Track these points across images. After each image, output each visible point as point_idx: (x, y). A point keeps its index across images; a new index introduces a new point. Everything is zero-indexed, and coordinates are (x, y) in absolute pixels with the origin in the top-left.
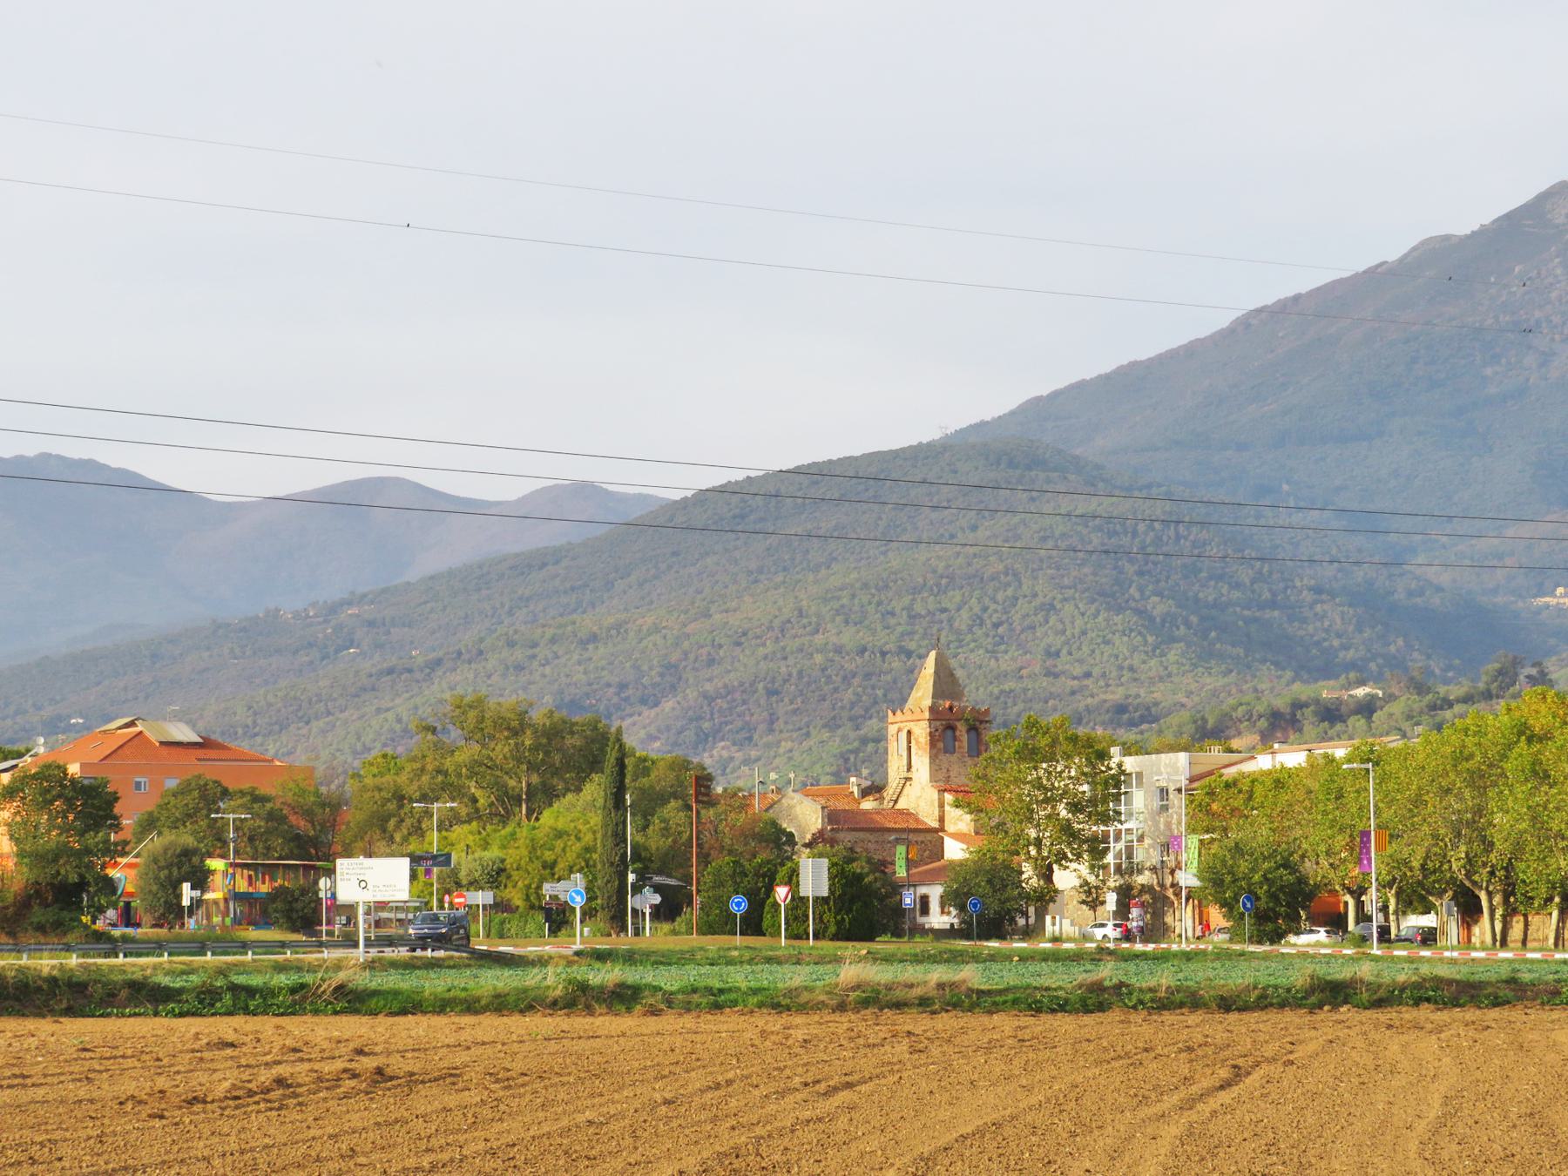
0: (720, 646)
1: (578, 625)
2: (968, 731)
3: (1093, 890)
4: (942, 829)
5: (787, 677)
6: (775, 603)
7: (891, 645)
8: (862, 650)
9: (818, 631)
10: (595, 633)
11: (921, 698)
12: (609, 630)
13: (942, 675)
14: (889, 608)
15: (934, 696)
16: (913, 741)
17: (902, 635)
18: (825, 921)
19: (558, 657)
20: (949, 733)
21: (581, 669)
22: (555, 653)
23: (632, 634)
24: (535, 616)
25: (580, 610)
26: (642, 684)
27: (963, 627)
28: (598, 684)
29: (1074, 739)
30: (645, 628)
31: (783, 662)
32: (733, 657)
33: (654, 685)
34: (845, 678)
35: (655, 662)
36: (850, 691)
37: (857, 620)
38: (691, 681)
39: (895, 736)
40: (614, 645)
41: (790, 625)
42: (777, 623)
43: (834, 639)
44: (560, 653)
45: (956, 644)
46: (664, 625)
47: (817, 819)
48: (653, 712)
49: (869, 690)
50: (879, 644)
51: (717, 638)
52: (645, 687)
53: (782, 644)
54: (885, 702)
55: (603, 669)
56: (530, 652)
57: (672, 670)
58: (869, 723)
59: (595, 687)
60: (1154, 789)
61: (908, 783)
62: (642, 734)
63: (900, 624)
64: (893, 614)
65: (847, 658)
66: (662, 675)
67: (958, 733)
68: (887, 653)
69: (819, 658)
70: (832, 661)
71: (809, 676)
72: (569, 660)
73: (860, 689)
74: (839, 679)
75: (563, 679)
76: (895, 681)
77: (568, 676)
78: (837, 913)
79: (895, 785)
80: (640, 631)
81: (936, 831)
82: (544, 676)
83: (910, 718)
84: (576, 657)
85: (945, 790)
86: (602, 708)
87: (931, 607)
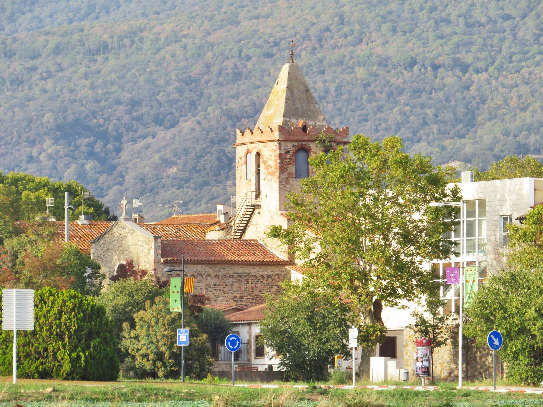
0: (249, 58)
1: (86, 32)
3: (430, 329)
4: (291, 263)
5: (323, 94)
6: (313, 8)
7: (445, 57)
8: (412, 63)
9: (361, 41)
10: (104, 42)
11: (271, 117)
12: (121, 38)
13: (296, 91)
14: (443, 15)
15: (286, 114)
16: (262, 165)
17: (458, 45)
18: (59, 359)
19: (62, 70)
20: (302, 155)
21: (87, 83)
22: (59, 64)
23: (148, 44)
24: (41, 21)
25: (93, 15)
26: (157, 100)
27: (529, 36)
28: (106, 100)
29: (404, 163)
30: (163, 37)
31: (319, 77)
32: (263, 71)
33: (171, 102)
34: (390, 95)
35: (173, 76)
36: (396, 109)
37: (406, 28)
38: (214, 97)
39: (244, 159)
40: (127, 56)
41: (328, 34)
42: (313, 31)
43: (379, 50)
44: (65, 64)
45: (519, 56)
46: (185, 32)
47: (149, 250)
48: (169, 134)
49: (418, 109)
50: (431, 55)
51: (244, 50)
52: (161, 105)
53: (319, 55)
54: (435, 123)
55: (112, 83)
56: (30, 64)
57: (193, 85)
58: (416, 146)
59: (103, 103)
60: (496, 218)
61: (257, 211)
62: (156, 158)
63: (456, 33)
64: (448, 21)
65: (393, 72)
66: (180, 91)
68: (439, 67)
69: (360, 72)
70: (376, 75)
71: (350, 93)
72: (74, 72)
73: (407, 108)
74: (384, 96)
75: (67, 95)
76: (448, 100)
77: (72, 91)
78: (72, 351)
79: (242, 212)
80: (157, 40)
81: (281, 264)
82: (45, 91)
83: (258, 139)
84: (82, 70)
86: (111, 128)
87: (493, 14)
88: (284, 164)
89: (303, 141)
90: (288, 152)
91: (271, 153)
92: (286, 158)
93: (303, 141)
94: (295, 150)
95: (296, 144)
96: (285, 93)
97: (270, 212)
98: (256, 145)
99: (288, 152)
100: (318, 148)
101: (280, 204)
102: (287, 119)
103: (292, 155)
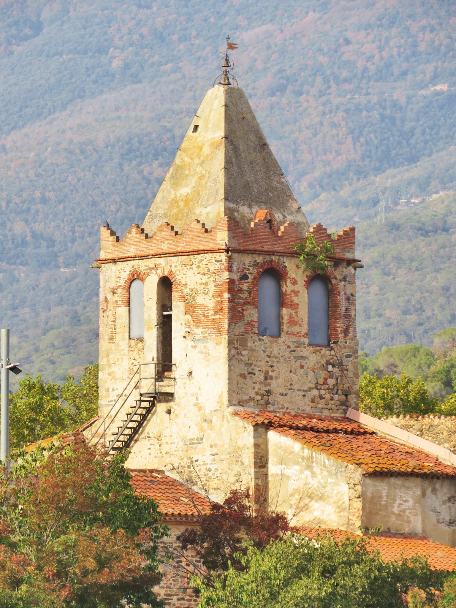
2: (310, 281)
61: (161, 408)
67: (287, 287)
85: (269, 425)
88: (238, 304)
89: (273, 253)
90: (244, 277)
91: (205, 279)
92: (241, 291)
93: (273, 253)
94: (258, 273)
95: (260, 259)
96: (222, 149)
97: (200, 408)
98: (161, 261)
99: (244, 277)
100: (300, 271)
101: (231, 391)
102: (232, 205)
103: (253, 283)
